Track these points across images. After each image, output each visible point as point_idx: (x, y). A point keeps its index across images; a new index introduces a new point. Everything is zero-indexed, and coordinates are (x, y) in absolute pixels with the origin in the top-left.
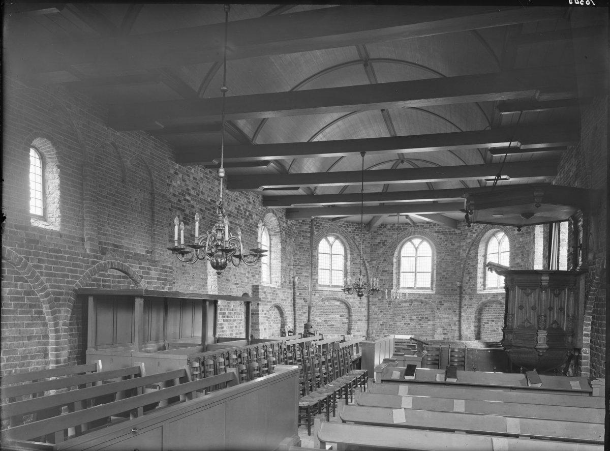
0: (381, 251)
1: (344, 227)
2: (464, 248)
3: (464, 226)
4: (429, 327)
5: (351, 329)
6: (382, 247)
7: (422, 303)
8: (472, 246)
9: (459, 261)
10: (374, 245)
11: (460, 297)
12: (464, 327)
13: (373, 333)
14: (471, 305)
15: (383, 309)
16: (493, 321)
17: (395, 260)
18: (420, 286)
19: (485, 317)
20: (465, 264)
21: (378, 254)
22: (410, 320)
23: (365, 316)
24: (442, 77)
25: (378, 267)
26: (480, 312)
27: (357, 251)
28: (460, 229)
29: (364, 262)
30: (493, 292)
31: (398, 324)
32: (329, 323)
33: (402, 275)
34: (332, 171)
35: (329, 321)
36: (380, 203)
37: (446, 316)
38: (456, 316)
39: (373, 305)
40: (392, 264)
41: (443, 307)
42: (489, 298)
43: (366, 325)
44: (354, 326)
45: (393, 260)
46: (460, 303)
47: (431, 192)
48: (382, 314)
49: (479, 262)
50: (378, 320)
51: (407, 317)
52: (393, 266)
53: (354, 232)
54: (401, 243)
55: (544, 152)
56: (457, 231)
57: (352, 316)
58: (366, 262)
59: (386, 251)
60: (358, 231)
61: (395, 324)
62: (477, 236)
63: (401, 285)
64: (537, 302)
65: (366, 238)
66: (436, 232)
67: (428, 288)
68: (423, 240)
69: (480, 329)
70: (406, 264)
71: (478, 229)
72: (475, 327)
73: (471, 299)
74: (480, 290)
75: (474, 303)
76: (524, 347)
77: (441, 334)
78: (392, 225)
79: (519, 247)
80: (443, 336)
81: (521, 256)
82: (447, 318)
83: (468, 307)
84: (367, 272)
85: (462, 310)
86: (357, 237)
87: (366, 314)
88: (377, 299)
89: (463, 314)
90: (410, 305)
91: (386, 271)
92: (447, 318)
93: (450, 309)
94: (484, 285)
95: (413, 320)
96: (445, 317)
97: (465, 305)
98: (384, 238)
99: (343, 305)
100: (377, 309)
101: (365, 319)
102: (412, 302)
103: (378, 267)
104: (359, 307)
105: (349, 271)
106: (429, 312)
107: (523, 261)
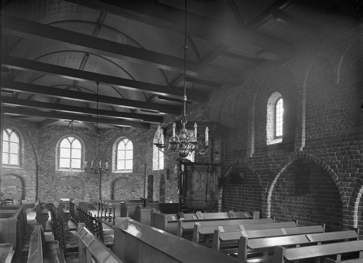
0: (46, 143)
1: (21, 123)
2: (103, 146)
3: (103, 132)
4: (80, 193)
5: (25, 196)
6: (47, 140)
7: (75, 178)
8: (108, 145)
9: (99, 153)
10: (41, 138)
11: (100, 174)
12: (103, 192)
13: (40, 198)
14: (108, 180)
15: (48, 182)
16: (122, 189)
17: (56, 150)
18: (73, 167)
19: (117, 187)
20: (103, 155)
21: (44, 144)
22: (67, 189)
23: (34, 187)
24: (141, 48)
25: (44, 153)
26: (113, 184)
27: (29, 141)
28: (100, 134)
29: (34, 149)
30: (122, 172)
31: (59, 191)
32: (8, 192)
33: (61, 159)
34: (32, 83)
35: (8, 190)
36: (52, 111)
37: (92, 186)
38: (97, 186)
39: (40, 179)
40: (55, 152)
41: (90, 181)
42: (120, 176)
43: (35, 193)
44: (27, 193)
45: (55, 149)
46: (100, 179)
47: (86, 109)
48: (47, 185)
49: (113, 154)
50: (45, 189)
51: (65, 187)
52: (55, 154)
53: (27, 128)
54: (61, 139)
55: (166, 100)
56: (98, 135)
57: (25, 186)
58: (36, 149)
59: (50, 143)
60: (30, 127)
61: (56, 191)
62: (112, 139)
63: (61, 166)
64: (205, 178)
65: (35, 133)
66: (85, 134)
67: (79, 169)
68: (75, 138)
69: (113, 193)
70: (120, 155)
71: (113, 136)
72: (111, 192)
73: (108, 176)
74: (113, 171)
75: (110, 178)
76: (200, 200)
77: (88, 197)
78: (54, 126)
79: (139, 148)
80: (90, 198)
81: (140, 153)
82: (92, 187)
83: (105, 181)
84: (36, 156)
85: (102, 182)
86: (29, 132)
87: (35, 185)
88: (43, 175)
89: (102, 185)
90: (67, 179)
91: (50, 156)
92: (92, 187)
93: (94, 182)
94: (116, 168)
95: (69, 189)
96: (90, 187)
97: (104, 179)
98: (49, 134)
99: (18, 179)
100: (43, 182)
101: (34, 188)
102: (69, 177)
103: (44, 153)
104: (30, 180)
105: (23, 155)
106: (79, 184)
107: (141, 156)
